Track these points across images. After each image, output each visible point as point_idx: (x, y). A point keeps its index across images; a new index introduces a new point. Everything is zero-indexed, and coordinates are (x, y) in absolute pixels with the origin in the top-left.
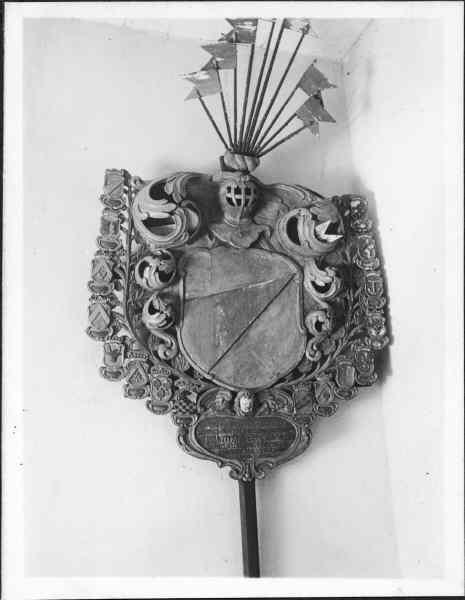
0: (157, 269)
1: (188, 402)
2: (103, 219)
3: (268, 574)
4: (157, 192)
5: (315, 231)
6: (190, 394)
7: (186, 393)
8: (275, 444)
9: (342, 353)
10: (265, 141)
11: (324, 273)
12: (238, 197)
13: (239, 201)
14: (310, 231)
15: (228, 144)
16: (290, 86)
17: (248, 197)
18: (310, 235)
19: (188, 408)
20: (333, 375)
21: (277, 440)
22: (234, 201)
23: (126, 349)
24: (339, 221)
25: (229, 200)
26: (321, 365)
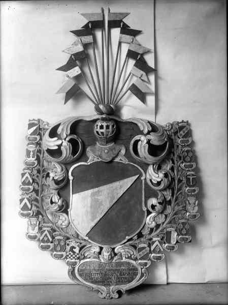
0: (53, 178)
1: (74, 253)
2: (27, 149)
3: (133, 68)
4: (53, 133)
5: (165, 221)
6: (75, 248)
7: (73, 247)
8: (126, 278)
9: (170, 222)
10: (115, 100)
11: (157, 176)
12: (102, 130)
13: (102, 133)
14: (144, 149)
15: (94, 100)
16: (132, 180)
17: (108, 130)
18: (145, 152)
19: (74, 256)
20: (166, 238)
21: (126, 276)
22: (100, 133)
23: (40, 223)
24: (165, 145)
25: (97, 132)
26: (156, 230)
